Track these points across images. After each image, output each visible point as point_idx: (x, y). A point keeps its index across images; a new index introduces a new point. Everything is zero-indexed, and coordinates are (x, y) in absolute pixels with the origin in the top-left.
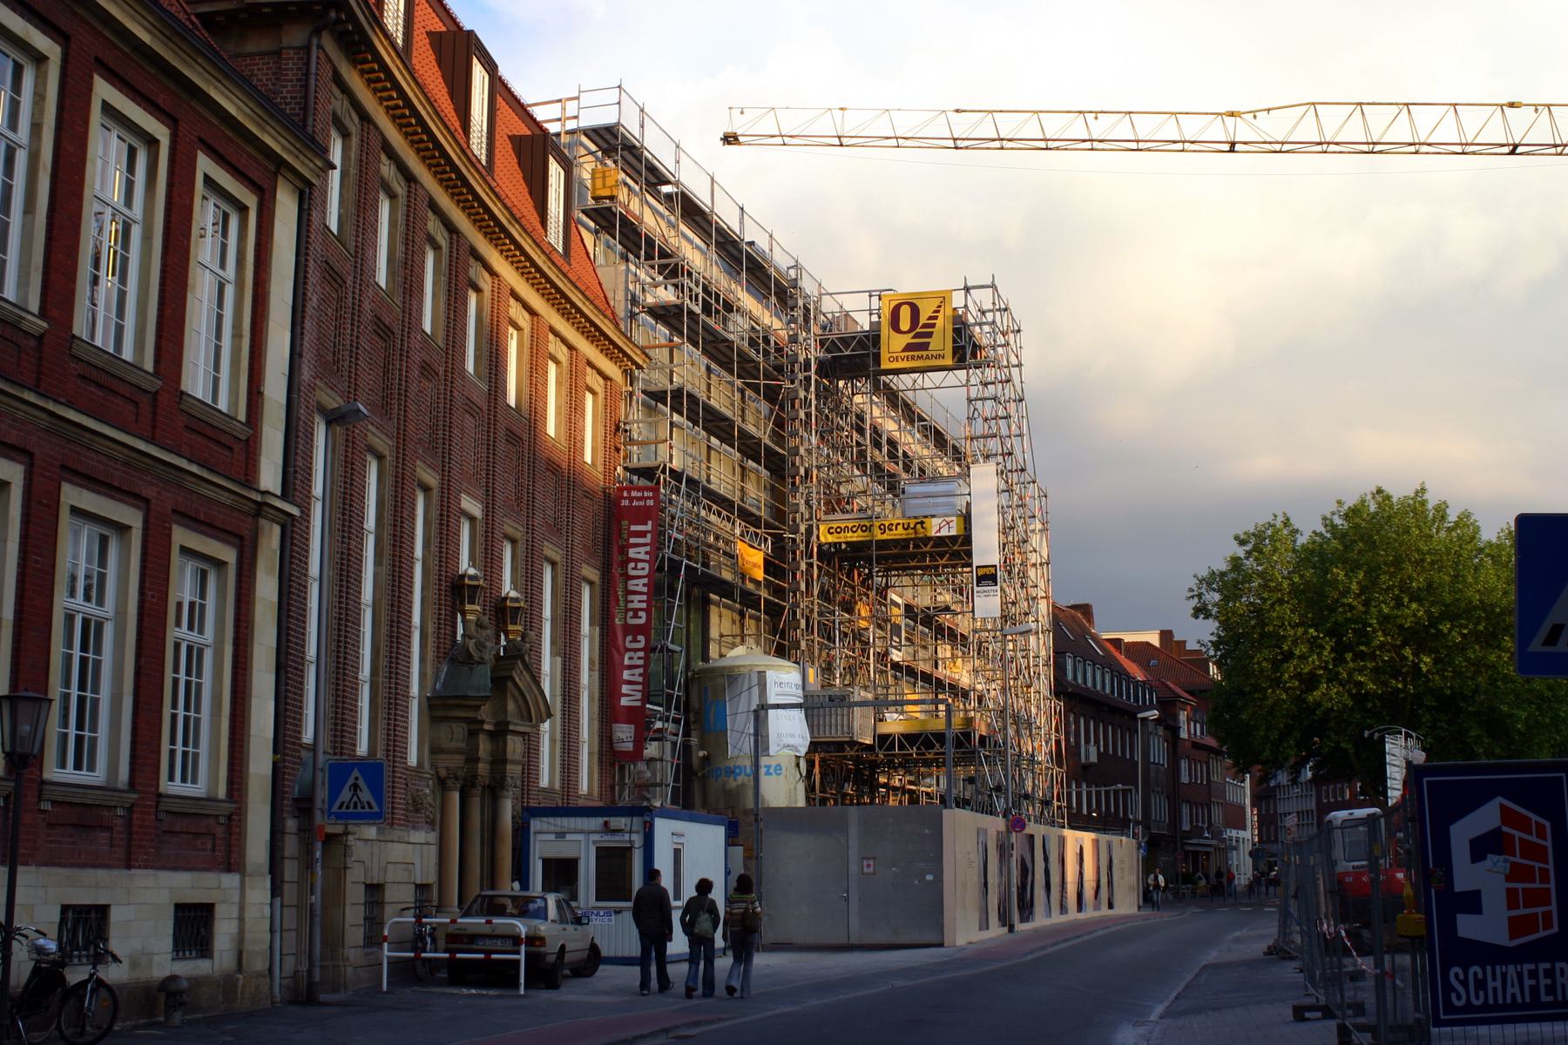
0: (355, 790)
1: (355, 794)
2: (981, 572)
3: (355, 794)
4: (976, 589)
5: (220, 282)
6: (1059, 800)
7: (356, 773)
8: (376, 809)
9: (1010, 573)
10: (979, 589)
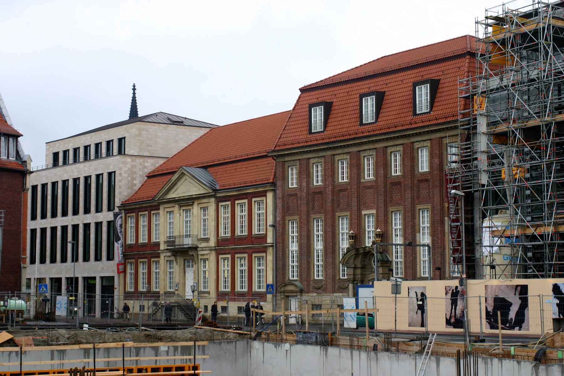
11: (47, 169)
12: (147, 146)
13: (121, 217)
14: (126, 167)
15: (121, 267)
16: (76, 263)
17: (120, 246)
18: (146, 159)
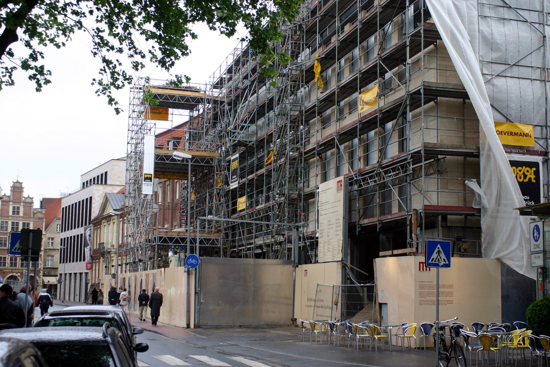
0: (439, 253)
1: (439, 255)
2: (146, 176)
3: (439, 255)
4: (144, 182)
5: (311, 54)
6: (206, 123)
7: (439, 246)
8: (447, 263)
9: (153, 54)
10: (145, 182)
11: (81, 190)
12: (119, 177)
13: (91, 229)
14: (98, 193)
15: (89, 266)
16: (66, 264)
17: (88, 250)
18: (114, 187)
